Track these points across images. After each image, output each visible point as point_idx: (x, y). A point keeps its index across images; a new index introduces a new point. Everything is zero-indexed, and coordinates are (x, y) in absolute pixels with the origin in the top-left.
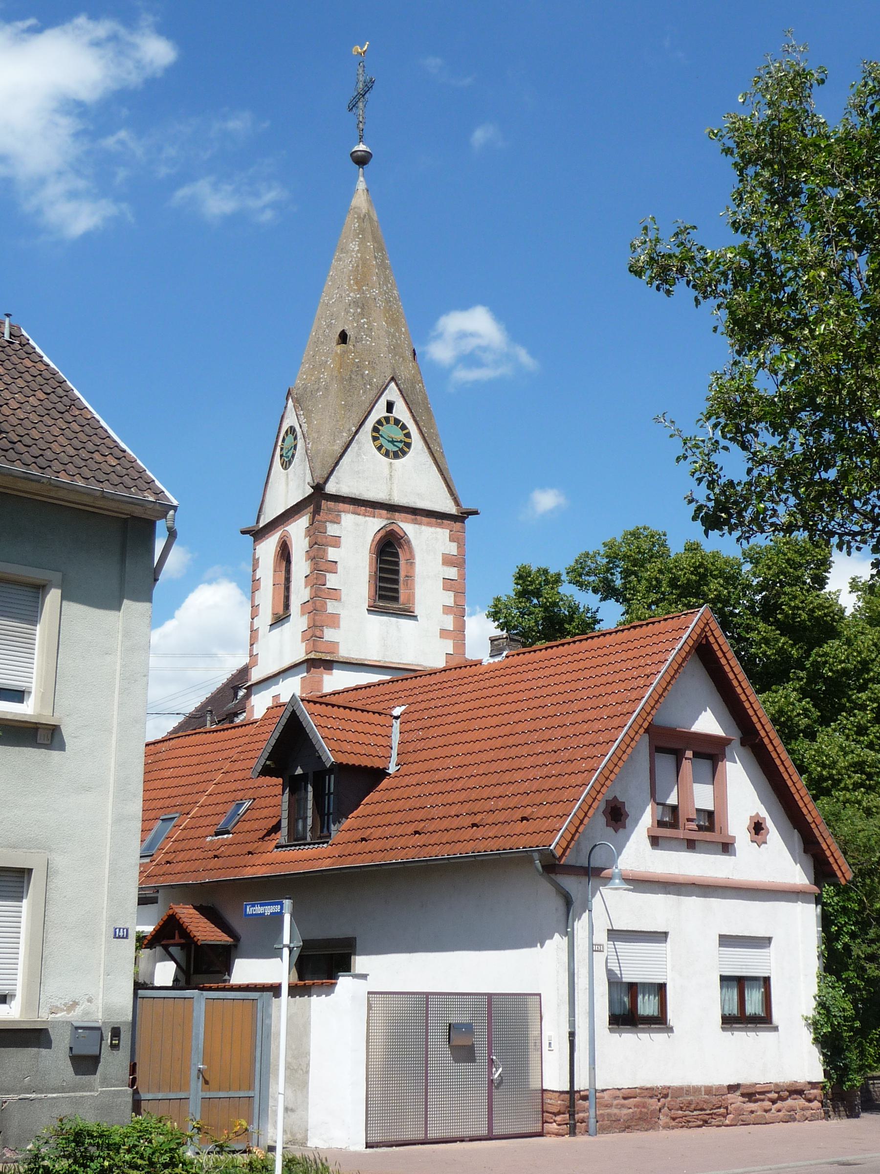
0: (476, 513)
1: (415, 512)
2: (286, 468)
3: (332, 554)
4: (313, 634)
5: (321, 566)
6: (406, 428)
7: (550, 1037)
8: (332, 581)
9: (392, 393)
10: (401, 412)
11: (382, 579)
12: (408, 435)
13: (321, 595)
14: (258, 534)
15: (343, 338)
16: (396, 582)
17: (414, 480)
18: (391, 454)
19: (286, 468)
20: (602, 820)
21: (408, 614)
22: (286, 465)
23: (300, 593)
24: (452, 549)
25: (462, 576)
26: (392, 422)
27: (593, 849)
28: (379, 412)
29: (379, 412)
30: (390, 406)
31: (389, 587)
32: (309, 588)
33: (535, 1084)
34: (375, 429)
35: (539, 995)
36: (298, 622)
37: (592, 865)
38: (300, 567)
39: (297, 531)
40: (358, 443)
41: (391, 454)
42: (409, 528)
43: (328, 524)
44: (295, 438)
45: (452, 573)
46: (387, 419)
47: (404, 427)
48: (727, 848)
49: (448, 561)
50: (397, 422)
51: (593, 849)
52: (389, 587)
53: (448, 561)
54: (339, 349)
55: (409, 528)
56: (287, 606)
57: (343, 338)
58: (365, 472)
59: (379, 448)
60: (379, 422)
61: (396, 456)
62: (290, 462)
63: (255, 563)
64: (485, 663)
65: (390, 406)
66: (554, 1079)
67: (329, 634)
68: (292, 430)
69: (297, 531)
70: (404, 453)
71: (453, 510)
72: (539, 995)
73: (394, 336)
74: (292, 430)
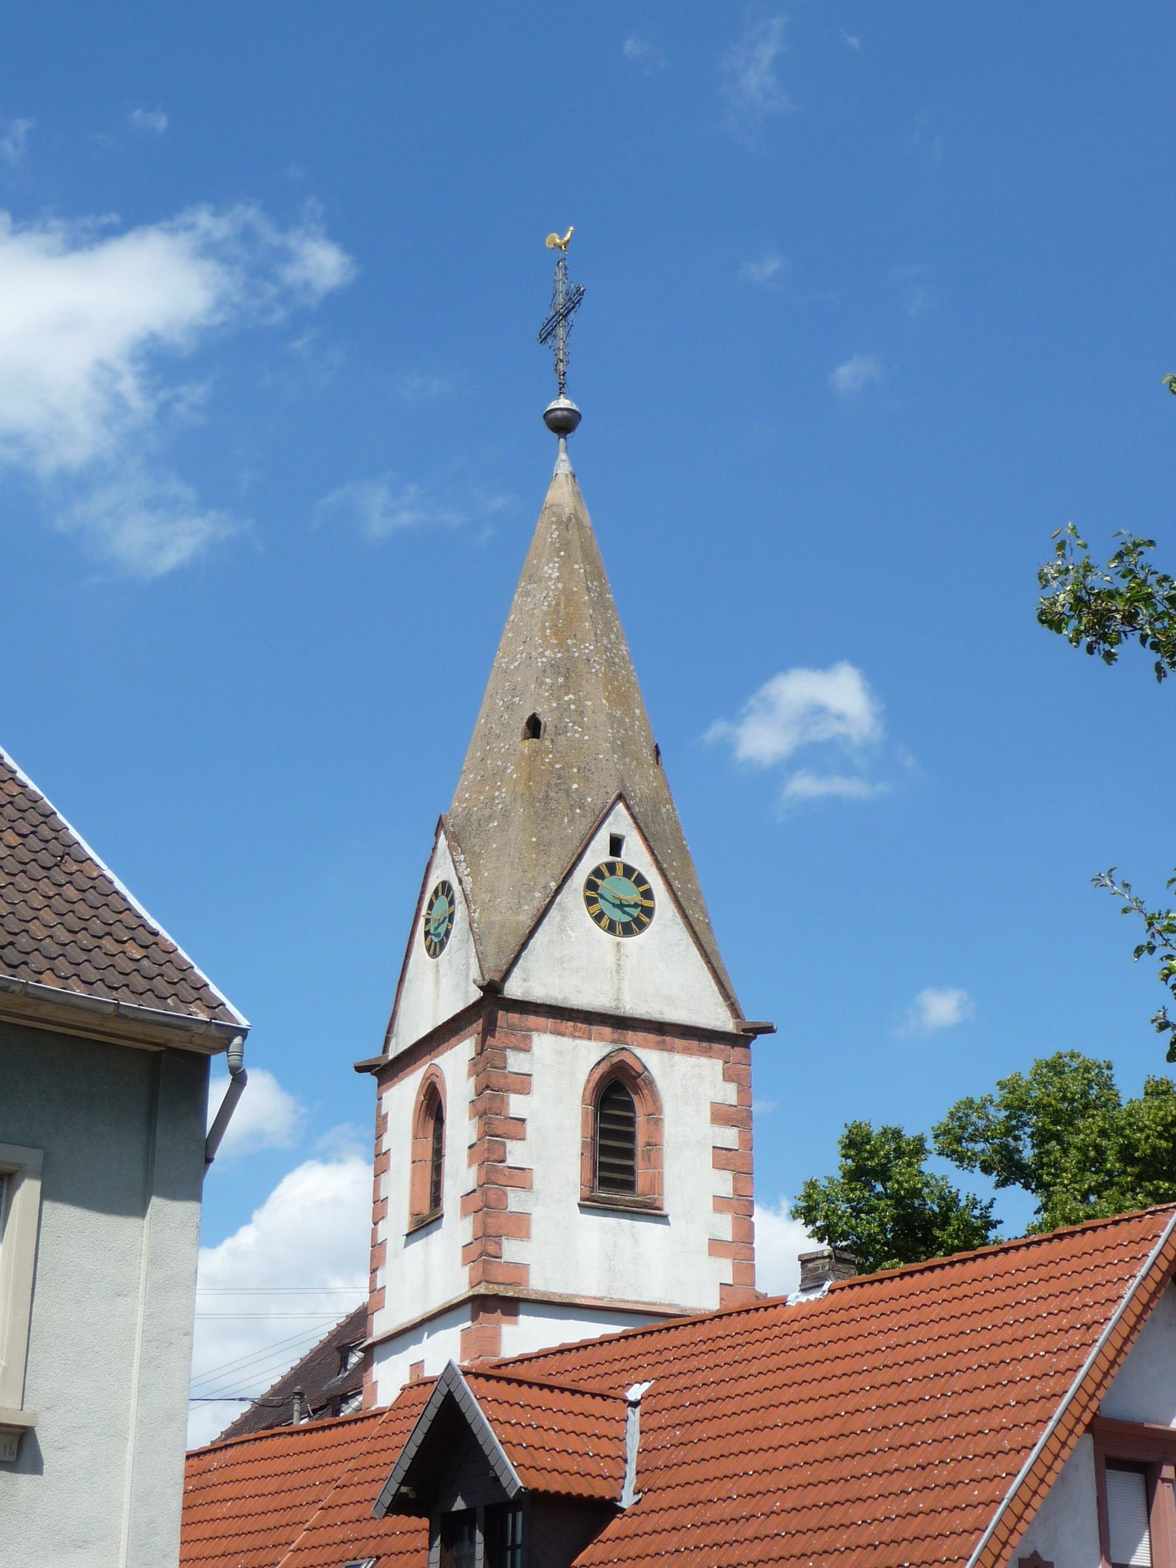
2: (434, 955)
3: (516, 1105)
4: (482, 1253)
5: (496, 1127)
8: (516, 1154)
9: (620, 822)
10: (635, 854)
12: (648, 895)
13: (497, 1178)
14: (386, 1071)
15: (534, 727)
18: (619, 928)
19: (434, 955)
22: (435, 948)
23: (460, 1176)
24: (729, 1094)
25: (747, 1143)
28: (598, 854)
29: (598, 854)
30: (616, 845)
31: (617, 1169)
34: (591, 885)
36: (456, 1229)
38: (460, 1129)
39: (455, 1064)
41: (619, 928)
42: (651, 1058)
43: (509, 1053)
45: (729, 1137)
46: (611, 867)
47: (640, 880)
50: (628, 871)
52: (617, 1169)
54: (527, 746)
55: (651, 1058)
57: (534, 727)
58: (572, 960)
59: (598, 918)
60: (597, 873)
61: (628, 931)
62: (442, 944)
65: (616, 845)
67: (512, 1251)
69: (455, 1064)
70: (642, 926)
73: (621, 723)
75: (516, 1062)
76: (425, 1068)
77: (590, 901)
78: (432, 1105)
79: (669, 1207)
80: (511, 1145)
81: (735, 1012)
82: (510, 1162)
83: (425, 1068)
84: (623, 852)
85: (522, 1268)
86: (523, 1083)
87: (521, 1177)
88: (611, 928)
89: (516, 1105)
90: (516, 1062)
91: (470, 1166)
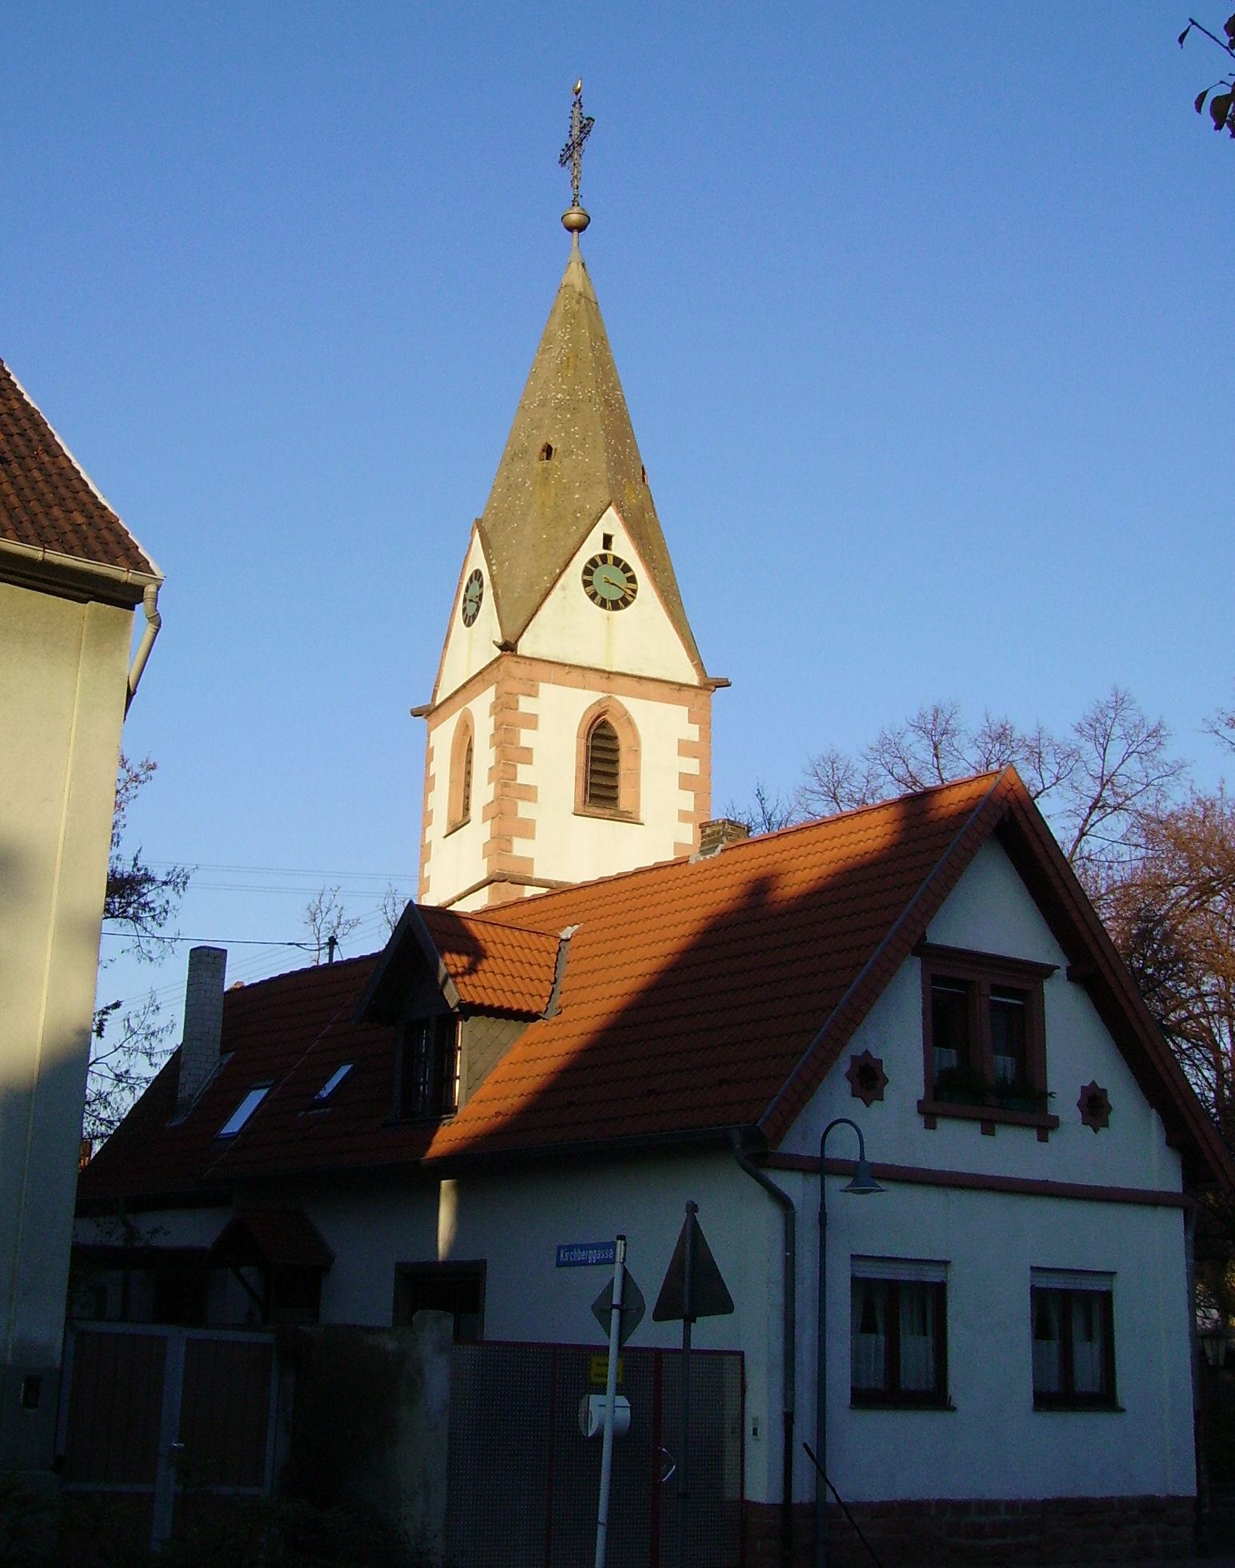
0: (726, 684)
1: (642, 683)
2: (469, 625)
3: (526, 737)
4: (500, 844)
5: (510, 754)
6: (630, 570)
7: (755, 1420)
8: (525, 775)
9: (611, 522)
10: (624, 548)
11: (593, 772)
12: (632, 579)
13: (509, 791)
14: (427, 713)
15: (548, 451)
16: (615, 775)
17: (644, 638)
18: (609, 605)
19: (469, 625)
20: (846, 1086)
21: (630, 818)
22: (469, 620)
23: (483, 792)
24: (693, 733)
25: (706, 769)
26: (610, 561)
27: (826, 1133)
28: (592, 547)
29: (592, 547)
30: (607, 540)
31: (603, 777)
32: (492, 785)
33: (731, 1493)
34: (587, 571)
35: (742, 1354)
36: (479, 830)
37: (828, 1155)
38: (484, 757)
39: (481, 705)
40: (563, 588)
41: (609, 605)
42: (633, 706)
43: (522, 698)
44: (481, 586)
45: (692, 766)
46: (604, 558)
47: (626, 569)
48: (1045, 1127)
49: (685, 749)
50: (617, 561)
51: (826, 1133)
52: (603, 777)
53: (685, 749)
54: (539, 465)
55: (633, 706)
56: (467, 809)
57: (548, 451)
58: (568, 625)
59: (593, 596)
60: (593, 562)
61: (616, 606)
62: (474, 617)
63: (429, 755)
64: (692, 861)
65: (607, 540)
66: (760, 1484)
67: (520, 847)
68: (477, 575)
69: (481, 705)
70: (627, 603)
71: (695, 680)
72: (742, 1354)
73: (616, 450)
74: (477, 575)
75: (525, 705)
76: (459, 713)
77: (587, 584)
78: (466, 729)
79: (643, 816)
80: (520, 804)
81: (700, 666)
82: (520, 780)
83: (459, 713)
84: (613, 547)
85: (530, 861)
86: (531, 721)
87: (529, 793)
88: (603, 604)
89: (526, 737)
90: (525, 705)
91: (484, 820)
